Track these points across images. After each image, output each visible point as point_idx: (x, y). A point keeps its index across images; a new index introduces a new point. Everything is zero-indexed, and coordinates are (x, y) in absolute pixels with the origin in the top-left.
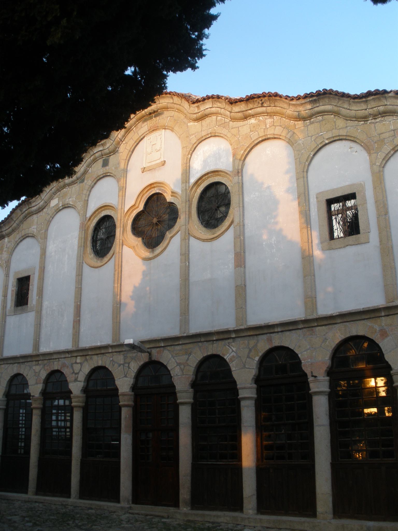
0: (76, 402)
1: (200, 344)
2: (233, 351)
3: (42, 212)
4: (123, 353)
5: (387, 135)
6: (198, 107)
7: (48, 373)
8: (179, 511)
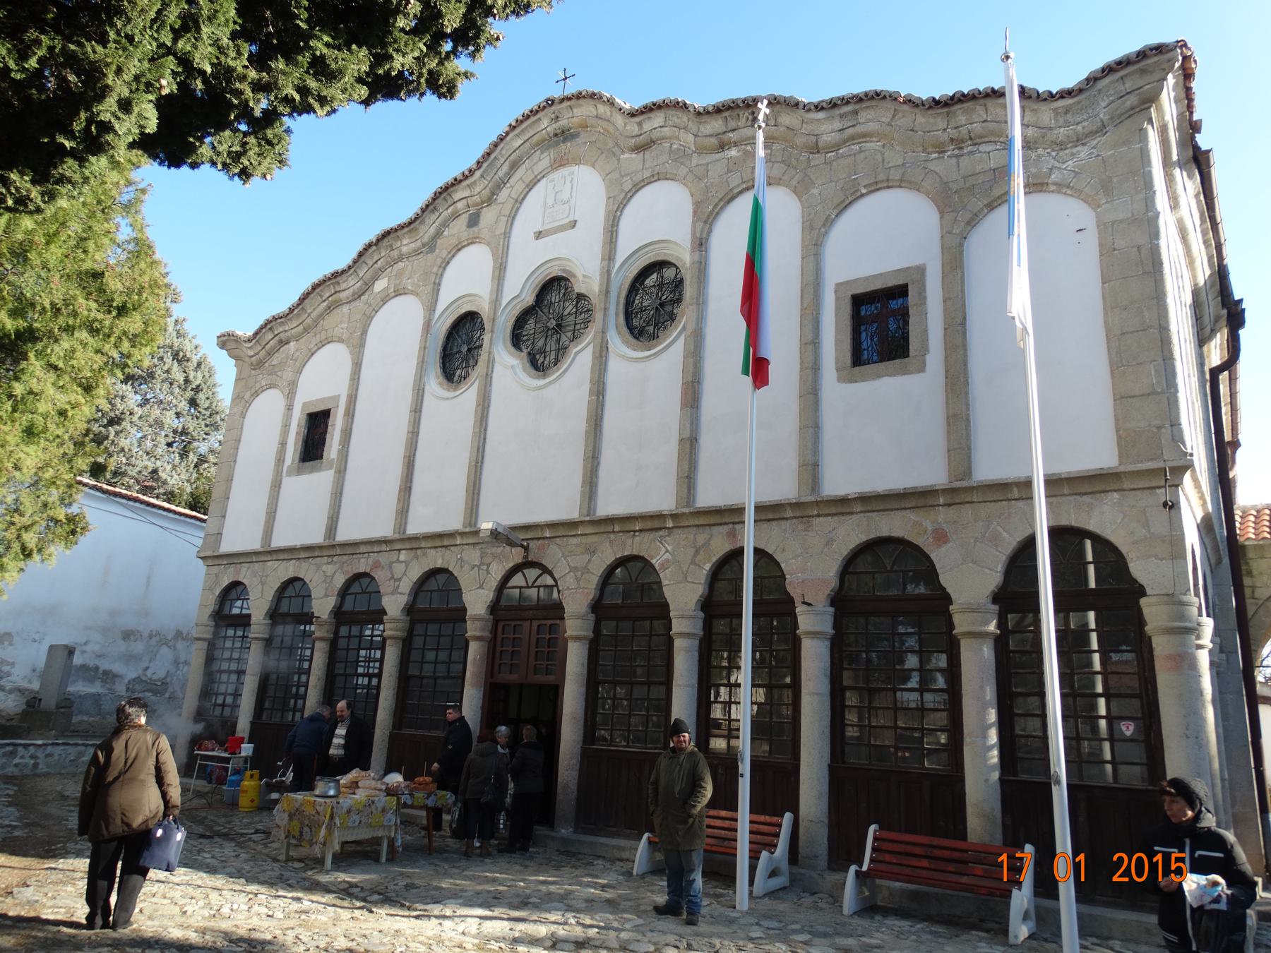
0: (391, 629)
1: (612, 536)
2: (667, 551)
3: (358, 301)
4: (480, 546)
5: (981, 178)
6: (640, 124)
7: (347, 577)
8: (553, 834)
